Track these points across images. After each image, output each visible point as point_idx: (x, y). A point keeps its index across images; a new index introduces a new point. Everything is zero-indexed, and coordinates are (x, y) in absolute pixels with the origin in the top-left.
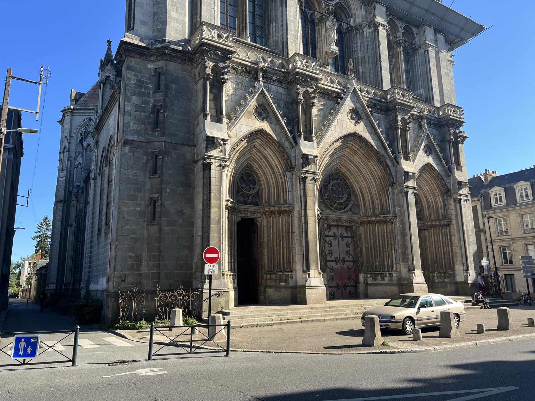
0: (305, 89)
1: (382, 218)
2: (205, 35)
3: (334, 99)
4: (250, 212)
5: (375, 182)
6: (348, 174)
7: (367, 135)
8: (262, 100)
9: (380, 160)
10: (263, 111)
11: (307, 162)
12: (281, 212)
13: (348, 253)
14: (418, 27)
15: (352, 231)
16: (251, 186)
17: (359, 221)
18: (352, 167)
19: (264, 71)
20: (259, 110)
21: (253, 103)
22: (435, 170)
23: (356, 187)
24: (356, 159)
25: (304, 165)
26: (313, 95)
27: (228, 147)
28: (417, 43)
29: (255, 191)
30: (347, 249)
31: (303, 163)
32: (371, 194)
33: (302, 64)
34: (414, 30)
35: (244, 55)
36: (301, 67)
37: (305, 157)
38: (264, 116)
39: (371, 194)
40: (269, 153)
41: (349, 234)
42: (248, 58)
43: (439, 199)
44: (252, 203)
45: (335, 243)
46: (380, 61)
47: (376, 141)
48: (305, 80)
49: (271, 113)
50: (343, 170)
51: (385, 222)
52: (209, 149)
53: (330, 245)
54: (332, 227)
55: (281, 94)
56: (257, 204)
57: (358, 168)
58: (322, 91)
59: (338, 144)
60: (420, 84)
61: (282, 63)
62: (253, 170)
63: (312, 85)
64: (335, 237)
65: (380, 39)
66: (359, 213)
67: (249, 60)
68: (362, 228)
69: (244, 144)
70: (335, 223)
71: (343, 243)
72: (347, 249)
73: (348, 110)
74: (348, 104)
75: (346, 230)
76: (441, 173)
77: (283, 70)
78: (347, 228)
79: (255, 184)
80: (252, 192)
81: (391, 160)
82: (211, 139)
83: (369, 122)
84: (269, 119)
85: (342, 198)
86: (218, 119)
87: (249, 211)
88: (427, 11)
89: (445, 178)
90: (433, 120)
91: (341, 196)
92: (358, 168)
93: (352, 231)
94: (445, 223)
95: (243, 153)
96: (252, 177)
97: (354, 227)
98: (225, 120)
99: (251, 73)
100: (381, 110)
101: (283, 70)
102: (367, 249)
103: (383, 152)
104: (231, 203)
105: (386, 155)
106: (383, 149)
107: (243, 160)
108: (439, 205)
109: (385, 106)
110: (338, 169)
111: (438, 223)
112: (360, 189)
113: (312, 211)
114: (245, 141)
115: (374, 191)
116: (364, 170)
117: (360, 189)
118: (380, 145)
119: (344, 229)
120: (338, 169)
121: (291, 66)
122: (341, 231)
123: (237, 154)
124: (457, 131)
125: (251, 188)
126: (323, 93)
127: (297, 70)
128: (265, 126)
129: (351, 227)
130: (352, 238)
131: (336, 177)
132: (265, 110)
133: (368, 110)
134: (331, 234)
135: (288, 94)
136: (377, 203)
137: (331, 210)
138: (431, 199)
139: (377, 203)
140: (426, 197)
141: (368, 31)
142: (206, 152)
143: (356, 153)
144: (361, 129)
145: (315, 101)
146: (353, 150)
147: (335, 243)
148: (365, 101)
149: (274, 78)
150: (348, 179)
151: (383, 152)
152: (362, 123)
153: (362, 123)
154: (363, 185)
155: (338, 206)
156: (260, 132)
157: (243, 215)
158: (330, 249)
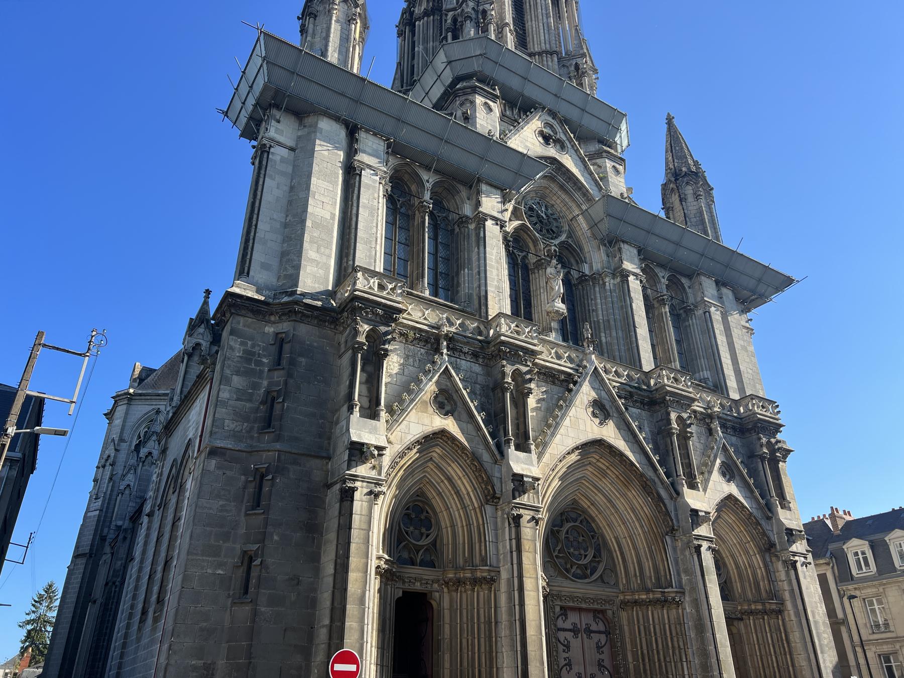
0: (515, 367)
1: (659, 596)
2: (359, 285)
3: (563, 384)
4: (420, 580)
5: (642, 527)
6: (593, 511)
7: (621, 444)
8: (445, 383)
9: (647, 487)
10: (446, 401)
11: (521, 489)
12: (475, 582)
13: (600, 665)
14: (690, 277)
15: (606, 621)
16: (423, 530)
17: (618, 601)
18: (600, 499)
19: (450, 339)
20: (440, 399)
21: (430, 388)
22: (743, 507)
23: (609, 536)
24: (605, 484)
25: (517, 494)
26: (528, 376)
27: (386, 461)
28: (691, 300)
29: (430, 539)
30: (599, 656)
31: (514, 490)
32: (635, 548)
33: (510, 328)
34: (684, 281)
35: (418, 315)
36: (508, 333)
37: (518, 479)
38: (448, 408)
39: (635, 548)
40: (455, 470)
41: (601, 627)
42: (425, 319)
43: (757, 560)
44: (423, 564)
45: (575, 643)
46: (635, 327)
47: (638, 456)
48: (515, 354)
49: (459, 404)
50: (585, 503)
51: (664, 602)
52: (353, 463)
53: (567, 647)
54: (569, 613)
55: (477, 374)
56: (431, 564)
57: (610, 501)
58: (543, 370)
59: (574, 457)
60: (703, 362)
61: (478, 327)
62: (427, 502)
63: (526, 361)
64: (575, 631)
65: (632, 295)
66: (616, 584)
67: (426, 322)
68: (624, 615)
69: (413, 454)
70: (575, 605)
71: (590, 644)
72: (599, 656)
73: (586, 402)
74: (586, 393)
75: (595, 617)
76: (755, 512)
77: (479, 338)
78: (598, 614)
79: (429, 528)
80: (424, 542)
81: (666, 489)
82: (358, 447)
83: (622, 423)
84: (456, 414)
85: (586, 556)
86: (371, 413)
87: (419, 577)
88: (293, 73)
89: (763, 522)
90: (730, 421)
91: (423, 530)
92: (610, 501)
93: (606, 621)
94: (774, 607)
95: (410, 471)
96: (425, 514)
97: (610, 613)
98: (384, 415)
99: (429, 341)
100: (642, 403)
101: (479, 338)
102: (635, 659)
103: (650, 473)
104: (387, 561)
105: (656, 480)
106: (650, 468)
107: (410, 482)
108: (759, 571)
109: (648, 397)
110: (575, 502)
111: (760, 607)
112: (617, 539)
113: (533, 580)
114: (415, 450)
115: (642, 544)
116: (621, 504)
117: (617, 539)
118: (644, 461)
119: (591, 615)
120: (575, 502)
121: (492, 332)
122: (586, 620)
123: (401, 472)
124: (383, 329)
125: (422, 534)
126: (545, 374)
127: (503, 338)
128: (450, 425)
129: (603, 612)
130: (607, 633)
131: (574, 515)
132: (449, 398)
133: (620, 402)
134: (568, 625)
135: (488, 374)
136: (648, 565)
137: (567, 578)
138: (742, 560)
139: (648, 565)
140: (733, 556)
141: (612, 281)
142: (348, 470)
143: (604, 474)
144: (610, 433)
145: (532, 385)
146: (599, 468)
147: (575, 643)
148: (614, 387)
149: (466, 350)
150: (594, 521)
151: (650, 473)
152: (611, 424)
153: (611, 424)
154: (621, 531)
155: (579, 571)
156: (442, 434)
157: (406, 586)
158: (566, 655)
